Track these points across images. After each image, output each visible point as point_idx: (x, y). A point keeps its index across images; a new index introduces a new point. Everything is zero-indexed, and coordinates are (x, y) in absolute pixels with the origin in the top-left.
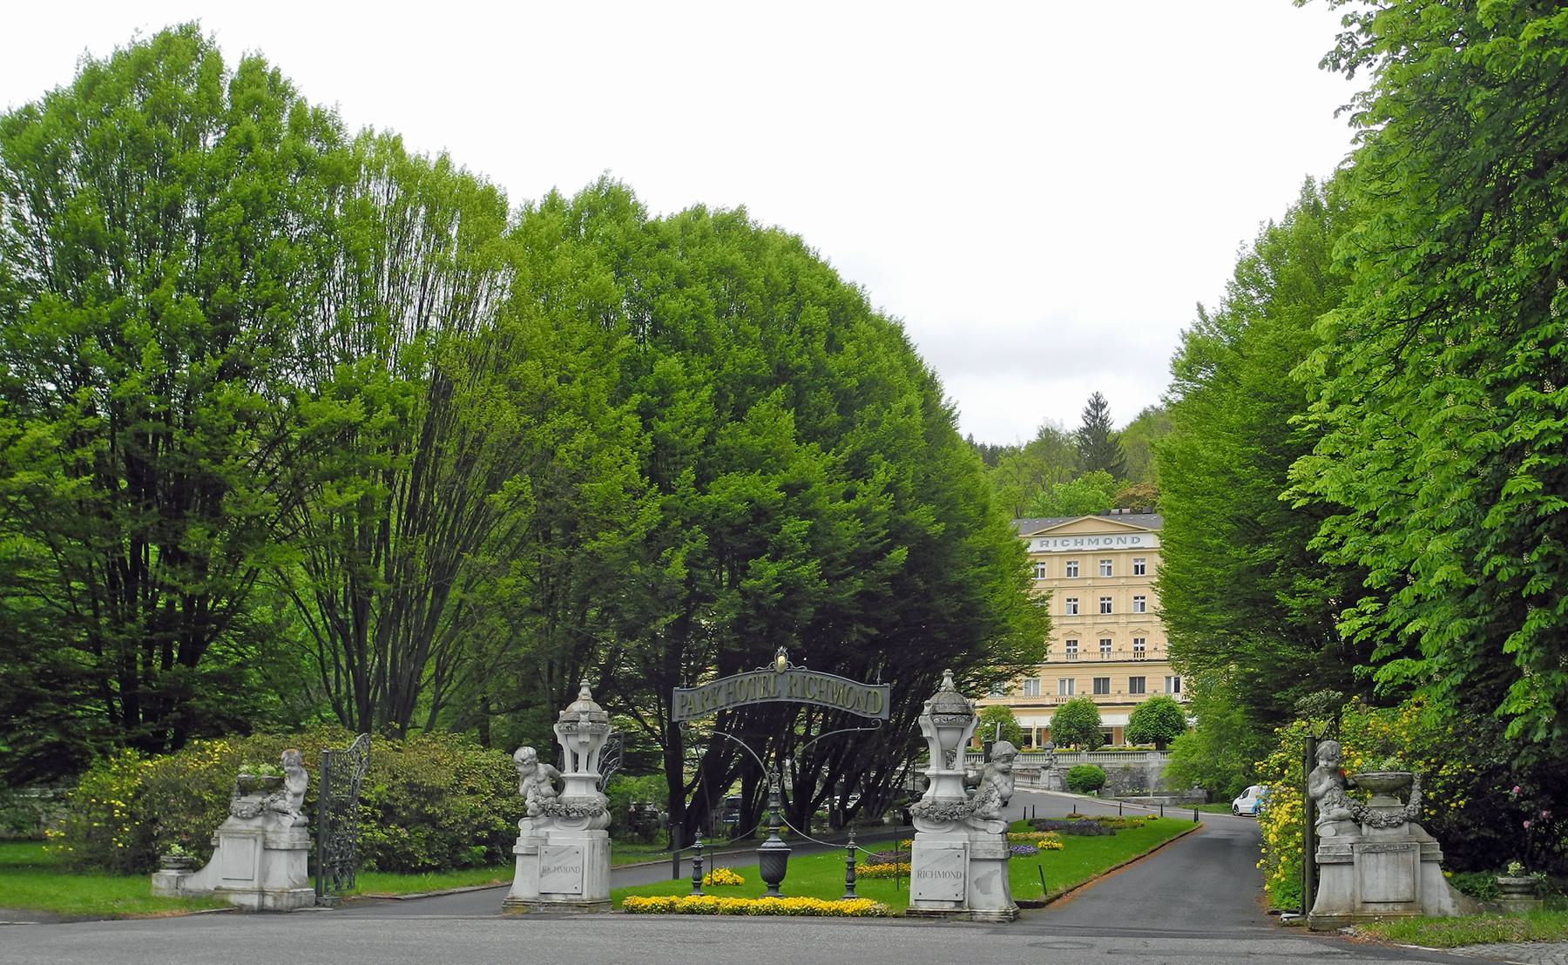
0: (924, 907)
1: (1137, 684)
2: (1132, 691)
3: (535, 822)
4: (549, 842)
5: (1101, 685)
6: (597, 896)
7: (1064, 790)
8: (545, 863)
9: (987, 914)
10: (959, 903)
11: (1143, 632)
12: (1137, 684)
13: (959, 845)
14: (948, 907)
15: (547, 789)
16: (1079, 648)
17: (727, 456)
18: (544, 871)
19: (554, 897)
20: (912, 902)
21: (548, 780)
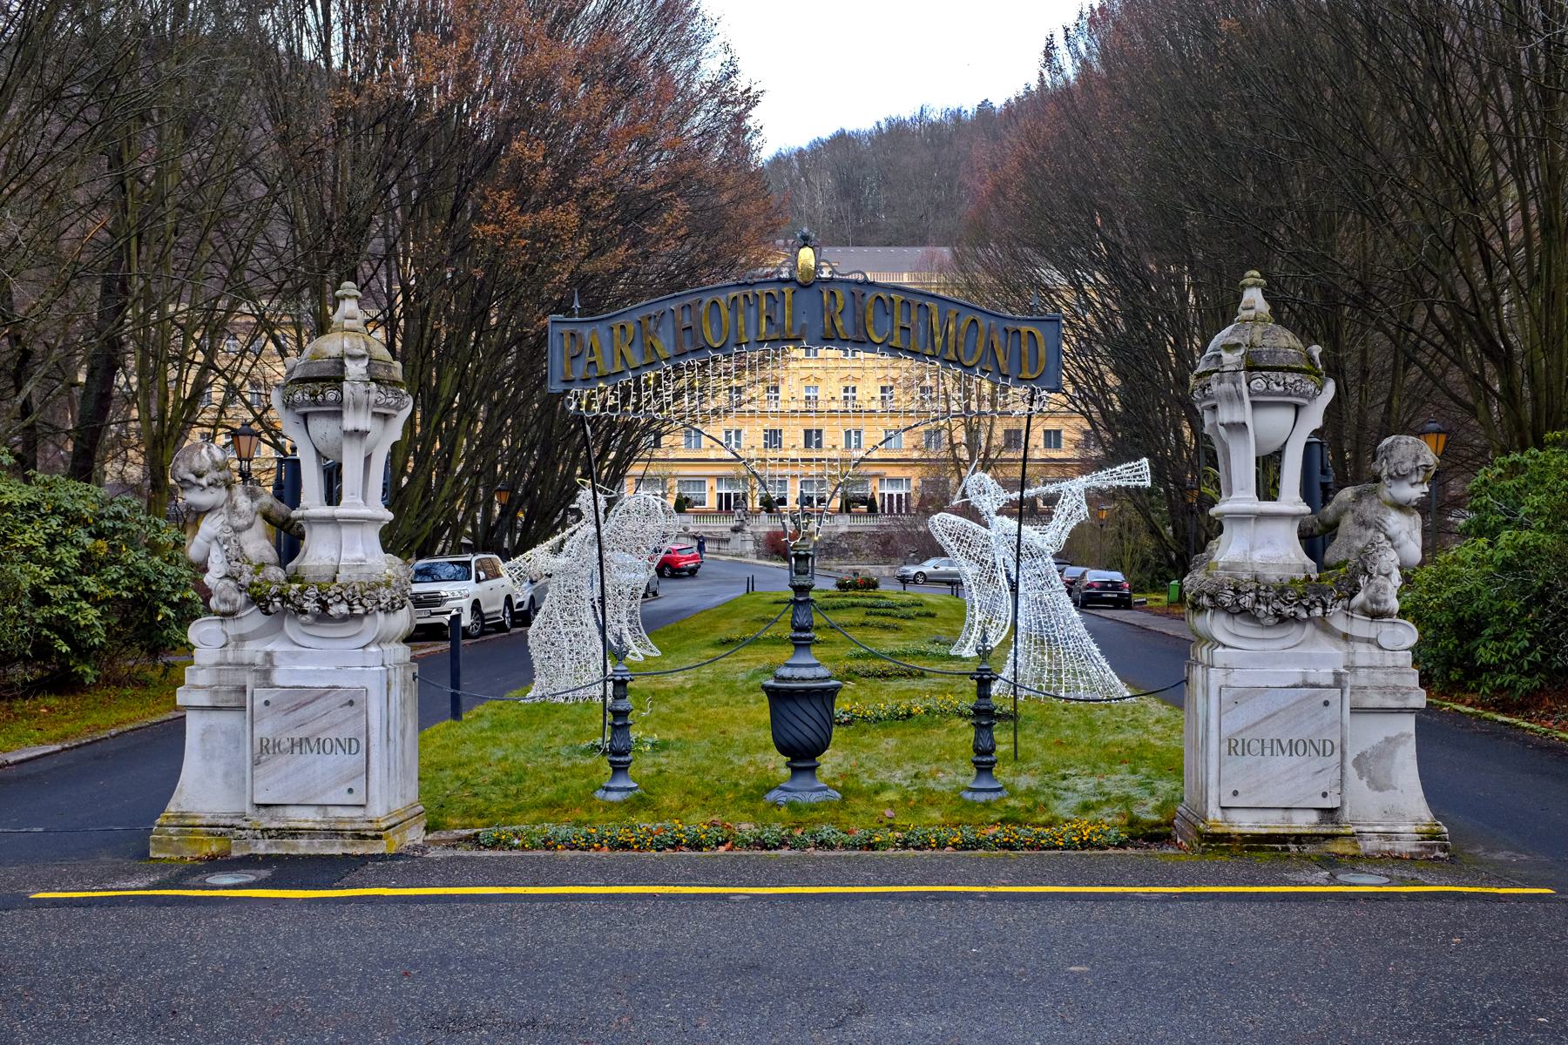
0: (1245, 823)
1: (812, 438)
2: (807, 444)
3: (232, 628)
4: (278, 678)
5: (773, 438)
6: (398, 805)
7: (758, 558)
8: (265, 729)
9: (1387, 836)
10: (1329, 814)
11: (854, 379)
12: (812, 438)
13: (1324, 675)
14: (1304, 822)
15: (258, 544)
16: (782, 394)
17: (233, 401)
18: (264, 748)
19: (291, 813)
20: (1214, 814)
21: (260, 524)
